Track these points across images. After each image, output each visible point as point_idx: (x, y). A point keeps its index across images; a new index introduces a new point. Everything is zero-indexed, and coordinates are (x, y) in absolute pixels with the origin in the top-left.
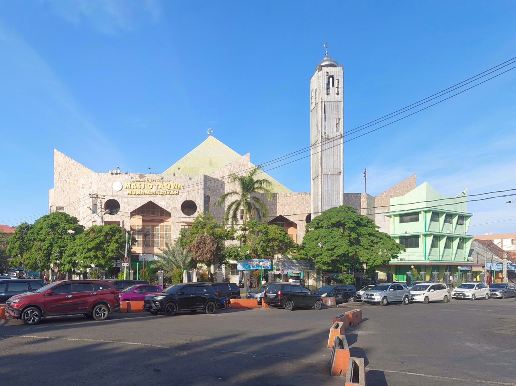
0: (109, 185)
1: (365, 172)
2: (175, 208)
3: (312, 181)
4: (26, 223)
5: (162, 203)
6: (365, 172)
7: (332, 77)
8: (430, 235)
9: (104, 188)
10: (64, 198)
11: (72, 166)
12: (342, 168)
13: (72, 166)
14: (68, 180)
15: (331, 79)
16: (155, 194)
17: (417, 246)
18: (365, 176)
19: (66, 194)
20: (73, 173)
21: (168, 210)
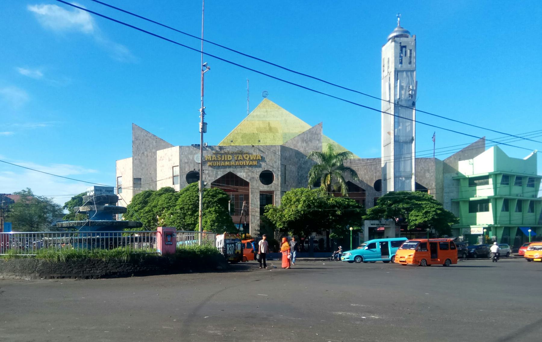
0: (191, 157)
1: (434, 136)
2: (253, 178)
3: (383, 148)
4: (29, 191)
5: (241, 174)
6: (434, 136)
7: (405, 47)
8: (500, 198)
9: (186, 161)
10: (142, 170)
11: (150, 139)
12: (414, 135)
13: (150, 139)
14: (145, 153)
15: (404, 49)
16: (236, 167)
17: (487, 210)
18: (434, 141)
19: (143, 166)
20: (151, 146)
21: (247, 180)
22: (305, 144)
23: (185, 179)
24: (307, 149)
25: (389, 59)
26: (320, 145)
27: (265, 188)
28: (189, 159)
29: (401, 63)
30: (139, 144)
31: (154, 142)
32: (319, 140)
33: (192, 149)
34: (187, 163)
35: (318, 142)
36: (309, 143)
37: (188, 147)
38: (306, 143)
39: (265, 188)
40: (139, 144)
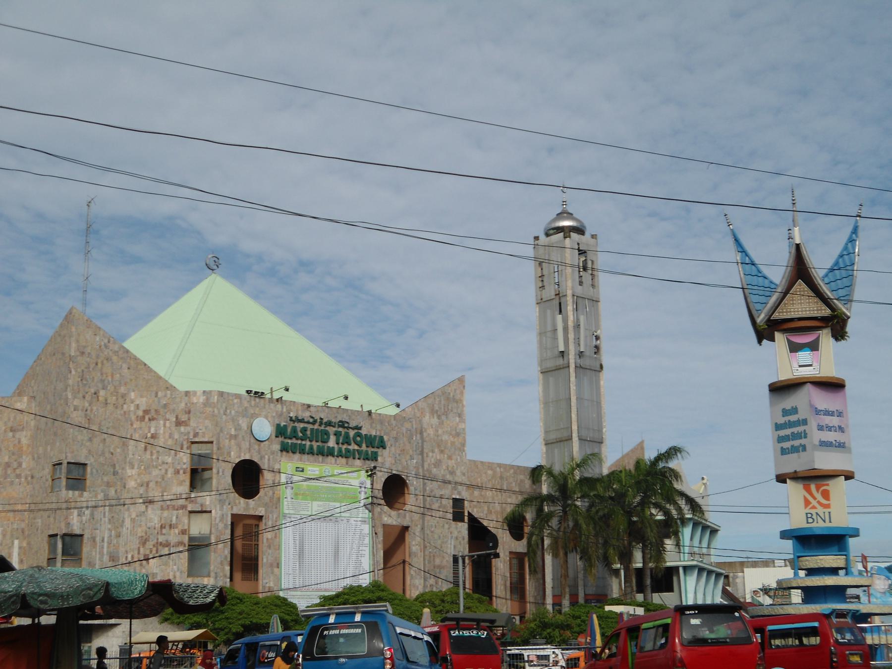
9: (233, 432)
10: (90, 440)
13: (115, 358)
14: (102, 393)
22: (435, 421)
23: (229, 480)
24: (440, 432)
25: (849, 513)
26: (462, 426)
27: (242, 506)
28: (238, 428)
29: (581, 283)
30: (88, 367)
31: (125, 366)
32: (460, 415)
33: (246, 404)
34: (236, 437)
35: (458, 419)
36: (443, 417)
37: (238, 396)
38: (439, 417)
39: (242, 506)
40: (88, 367)
